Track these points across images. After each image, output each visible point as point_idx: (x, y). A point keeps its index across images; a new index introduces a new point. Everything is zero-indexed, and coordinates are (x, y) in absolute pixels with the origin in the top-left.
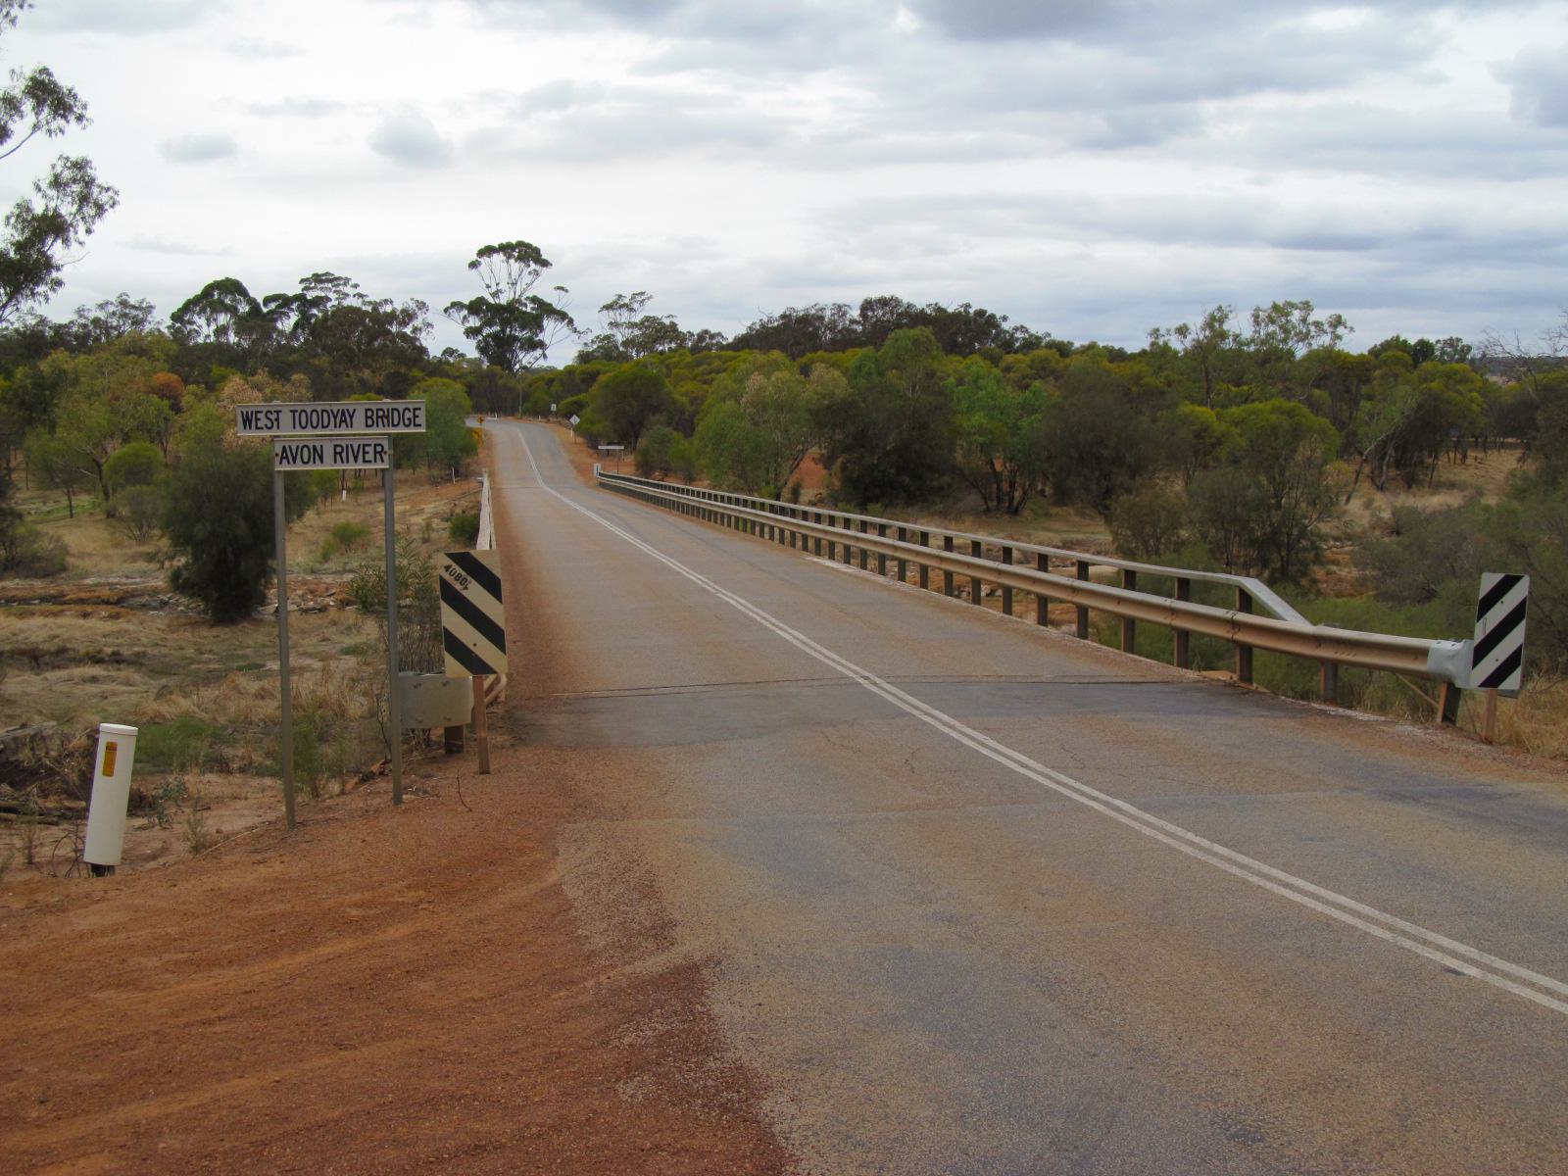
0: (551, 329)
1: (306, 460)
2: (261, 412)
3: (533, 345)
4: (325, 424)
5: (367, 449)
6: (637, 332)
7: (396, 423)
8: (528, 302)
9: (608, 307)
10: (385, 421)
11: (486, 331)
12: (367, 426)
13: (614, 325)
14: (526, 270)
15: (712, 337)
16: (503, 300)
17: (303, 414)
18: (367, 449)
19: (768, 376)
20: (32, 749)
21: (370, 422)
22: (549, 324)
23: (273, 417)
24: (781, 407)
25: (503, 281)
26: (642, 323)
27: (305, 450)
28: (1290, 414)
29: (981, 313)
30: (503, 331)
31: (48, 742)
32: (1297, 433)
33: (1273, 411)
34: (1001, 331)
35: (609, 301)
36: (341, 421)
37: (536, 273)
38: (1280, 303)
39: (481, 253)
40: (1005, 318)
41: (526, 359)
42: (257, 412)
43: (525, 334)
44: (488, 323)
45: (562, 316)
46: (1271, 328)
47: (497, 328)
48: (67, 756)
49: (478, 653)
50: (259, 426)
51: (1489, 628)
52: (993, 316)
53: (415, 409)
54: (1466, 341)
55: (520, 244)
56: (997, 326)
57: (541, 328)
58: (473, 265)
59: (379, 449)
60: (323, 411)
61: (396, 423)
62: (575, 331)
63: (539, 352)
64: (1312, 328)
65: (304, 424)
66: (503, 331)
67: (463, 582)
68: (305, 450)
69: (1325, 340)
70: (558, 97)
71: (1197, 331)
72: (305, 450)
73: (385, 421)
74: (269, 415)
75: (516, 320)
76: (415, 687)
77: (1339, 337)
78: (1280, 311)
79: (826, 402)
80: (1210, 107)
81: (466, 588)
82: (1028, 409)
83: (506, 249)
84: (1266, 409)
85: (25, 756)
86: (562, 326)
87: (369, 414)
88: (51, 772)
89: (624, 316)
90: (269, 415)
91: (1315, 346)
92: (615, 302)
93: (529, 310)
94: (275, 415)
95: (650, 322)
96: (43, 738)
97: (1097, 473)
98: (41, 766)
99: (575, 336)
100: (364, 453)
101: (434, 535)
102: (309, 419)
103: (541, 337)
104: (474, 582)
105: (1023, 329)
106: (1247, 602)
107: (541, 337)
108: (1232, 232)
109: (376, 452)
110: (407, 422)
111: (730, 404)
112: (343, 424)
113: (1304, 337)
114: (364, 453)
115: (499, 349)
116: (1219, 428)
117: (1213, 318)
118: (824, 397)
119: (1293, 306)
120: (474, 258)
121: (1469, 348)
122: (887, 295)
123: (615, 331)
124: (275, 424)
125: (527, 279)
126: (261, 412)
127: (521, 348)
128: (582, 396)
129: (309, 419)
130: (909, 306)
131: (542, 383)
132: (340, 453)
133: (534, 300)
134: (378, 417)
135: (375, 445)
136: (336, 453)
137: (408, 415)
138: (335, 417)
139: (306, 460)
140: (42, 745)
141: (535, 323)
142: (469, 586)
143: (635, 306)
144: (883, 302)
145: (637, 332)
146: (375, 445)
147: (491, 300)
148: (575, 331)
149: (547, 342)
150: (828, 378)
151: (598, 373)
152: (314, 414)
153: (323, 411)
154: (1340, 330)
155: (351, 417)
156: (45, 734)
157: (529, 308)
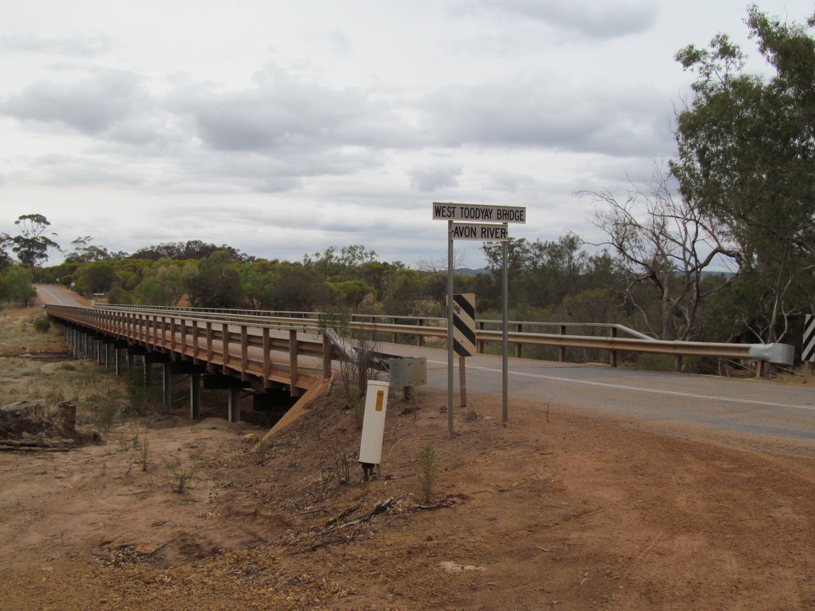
0: (50, 250)
1: (467, 235)
2: (445, 207)
3: (42, 256)
4: (478, 216)
5: (498, 231)
6: (87, 252)
7: (512, 217)
8: (40, 239)
9: (75, 242)
10: (507, 217)
11: (22, 249)
12: (498, 218)
13: (78, 249)
14: (40, 226)
15: (123, 254)
16: (30, 237)
17: (467, 210)
18: (498, 231)
19: (167, 267)
20: (36, 413)
21: (499, 216)
22: (49, 247)
23: (451, 210)
24: (172, 279)
25: (30, 229)
26: (89, 248)
27: (467, 229)
28: (360, 285)
29: (229, 248)
30: (29, 250)
31: (43, 410)
32: (364, 292)
33: (354, 284)
34: (237, 255)
35: (75, 239)
36: (485, 215)
37: (44, 227)
38: (353, 246)
39: (21, 218)
40: (238, 250)
41: (38, 261)
42: (443, 207)
43: (39, 251)
44: (23, 246)
45: (55, 244)
46: (349, 255)
47: (27, 249)
48: (53, 416)
49: (464, 347)
50: (444, 214)
51: (807, 337)
52: (234, 249)
53: (521, 211)
54: (403, 263)
55: (37, 215)
56: (236, 253)
57: (45, 249)
58: (17, 222)
59: (503, 231)
60: (477, 209)
61: (512, 217)
62: (61, 251)
63: (44, 259)
64: (364, 255)
65: (467, 216)
66: (29, 250)
67: (458, 310)
68: (467, 229)
69: (369, 259)
70: (51, 160)
71: (323, 256)
72: (467, 229)
73: (507, 217)
74: (449, 209)
75: (35, 246)
76: (408, 365)
77: (373, 258)
78: (352, 249)
79: (191, 278)
80: (304, 179)
81: (459, 313)
82: (267, 282)
83: (31, 217)
84: (351, 283)
85: (32, 417)
86: (55, 249)
87: (499, 212)
88: (48, 425)
89: (82, 246)
90: (449, 209)
91: (365, 262)
92: (78, 240)
93: (41, 242)
94: (452, 209)
95: (93, 248)
96: (41, 408)
97: (296, 306)
98: (43, 422)
99: (61, 253)
100: (496, 233)
101: (28, 329)
102: (470, 213)
103: (45, 253)
104: (463, 310)
105: (245, 254)
106: (615, 332)
107: (45, 253)
108: (308, 224)
109: (502, 233)
110: (517, 218)
111: (151, 278)
112: (486, 217)
113: (361, 258)
114: (496, 233)
115: (27, 257)
116: (336, 290)
117: (329, 250)
118: (191, 276)
119: (357, 247)
120: (17, 219)
121: (404, 265)
122: (197, 239)
123: (77, 251)
124: (452, 214)
125: (41, 229)
126: (445, 207)
127: (37, 257)
128: (70, 276)
129: (470, 213)
130: (205, 244)
131: (49, 271)
132: (484, 232)
133: (43, 238)
134: (503, 214)
135: (502, 229)
136: (482, 232)
137: (518, 214)
138: (483, 213)
139: (467, 235)
140: (40, 411)
141: (43, 247)
142: (461, 312)
143: (86, 242)
144: (196, 242)
145: (87, 252)
146: (502, 229)
147: (24, 237)
148: (61, 251)
149: (48, 255)
150: (191, 267)
151: (76, 267)
152: (472, 210)
153: (477, 209)
154: (374, 256)
155: (490, 213)
156: (41, 405)
157: (41, 241)
